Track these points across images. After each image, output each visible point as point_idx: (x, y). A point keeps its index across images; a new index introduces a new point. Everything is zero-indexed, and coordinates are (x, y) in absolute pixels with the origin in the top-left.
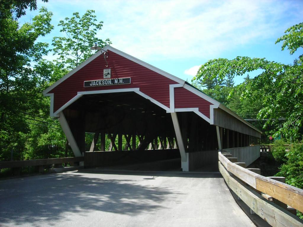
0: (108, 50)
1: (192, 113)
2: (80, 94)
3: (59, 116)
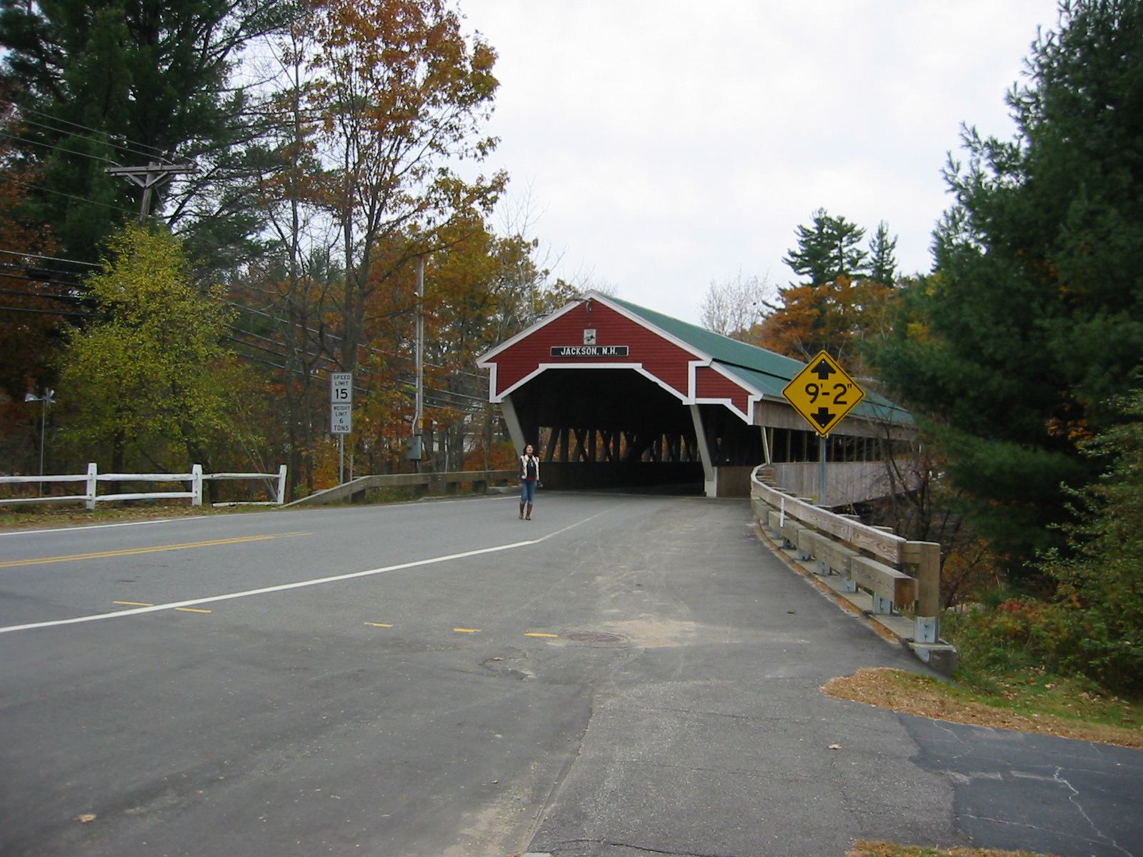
0: (591, 299)
2: (543, 367)
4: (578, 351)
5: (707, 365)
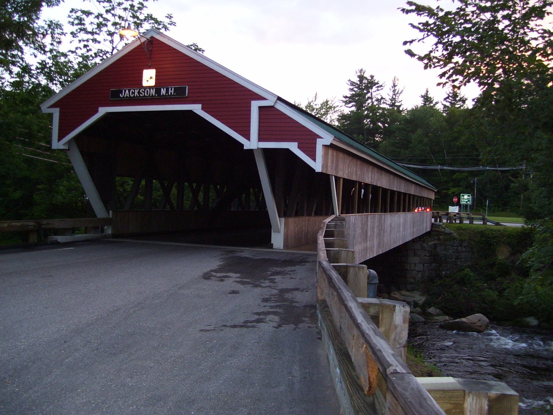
1: (287, 151)
2: (103, 111)
3: (67, 148)
4: (136, 93)
5: (272, 104)
